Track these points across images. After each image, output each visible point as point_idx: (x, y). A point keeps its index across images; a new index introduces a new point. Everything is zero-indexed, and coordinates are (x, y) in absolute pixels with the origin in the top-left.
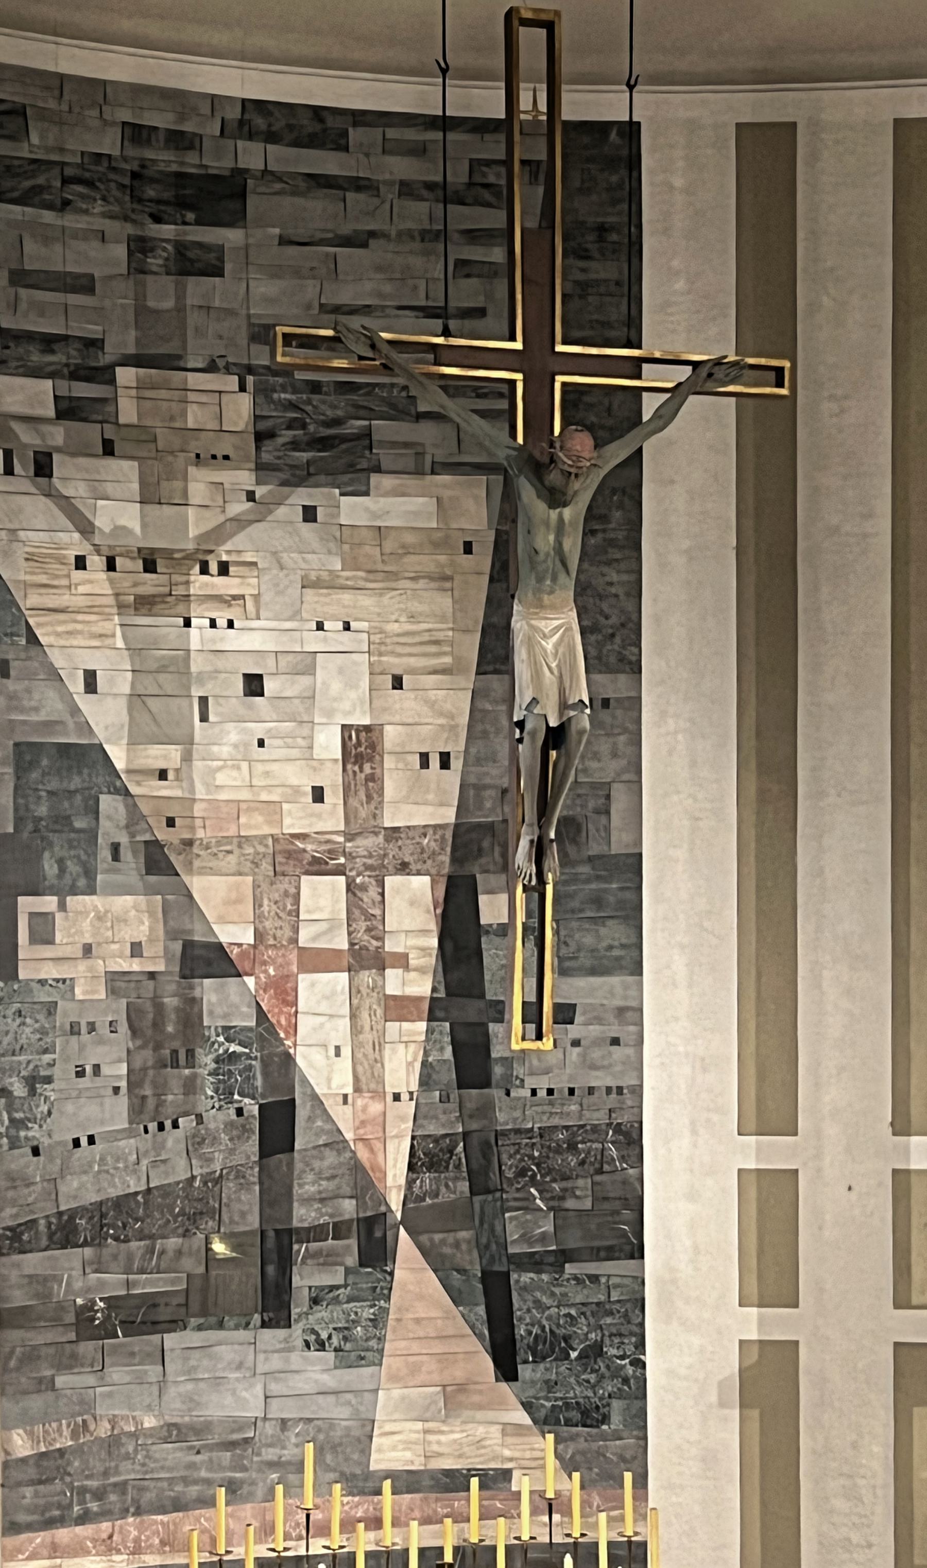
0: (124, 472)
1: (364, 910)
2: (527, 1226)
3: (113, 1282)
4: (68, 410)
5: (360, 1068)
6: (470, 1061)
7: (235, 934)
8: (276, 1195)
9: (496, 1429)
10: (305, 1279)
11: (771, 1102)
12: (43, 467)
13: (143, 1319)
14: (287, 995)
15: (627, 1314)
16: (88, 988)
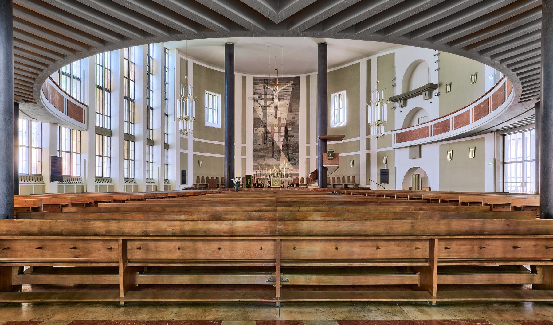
0: (263, 101)
1: (279, 129)
2: (291, 151)
3: (261, 154)
4: (259, 97)
5: (279, 141)
6: (287, 139)
7: (270, 131)
8: (273, 149)
9: (289, 165)
10: (274, 154)
11: (308, 141)
12: (257, 101)
13: (264, 156)
14: (273, 135)
15: (298, 157)
16: (259, 134)
